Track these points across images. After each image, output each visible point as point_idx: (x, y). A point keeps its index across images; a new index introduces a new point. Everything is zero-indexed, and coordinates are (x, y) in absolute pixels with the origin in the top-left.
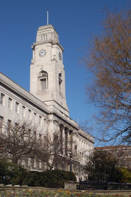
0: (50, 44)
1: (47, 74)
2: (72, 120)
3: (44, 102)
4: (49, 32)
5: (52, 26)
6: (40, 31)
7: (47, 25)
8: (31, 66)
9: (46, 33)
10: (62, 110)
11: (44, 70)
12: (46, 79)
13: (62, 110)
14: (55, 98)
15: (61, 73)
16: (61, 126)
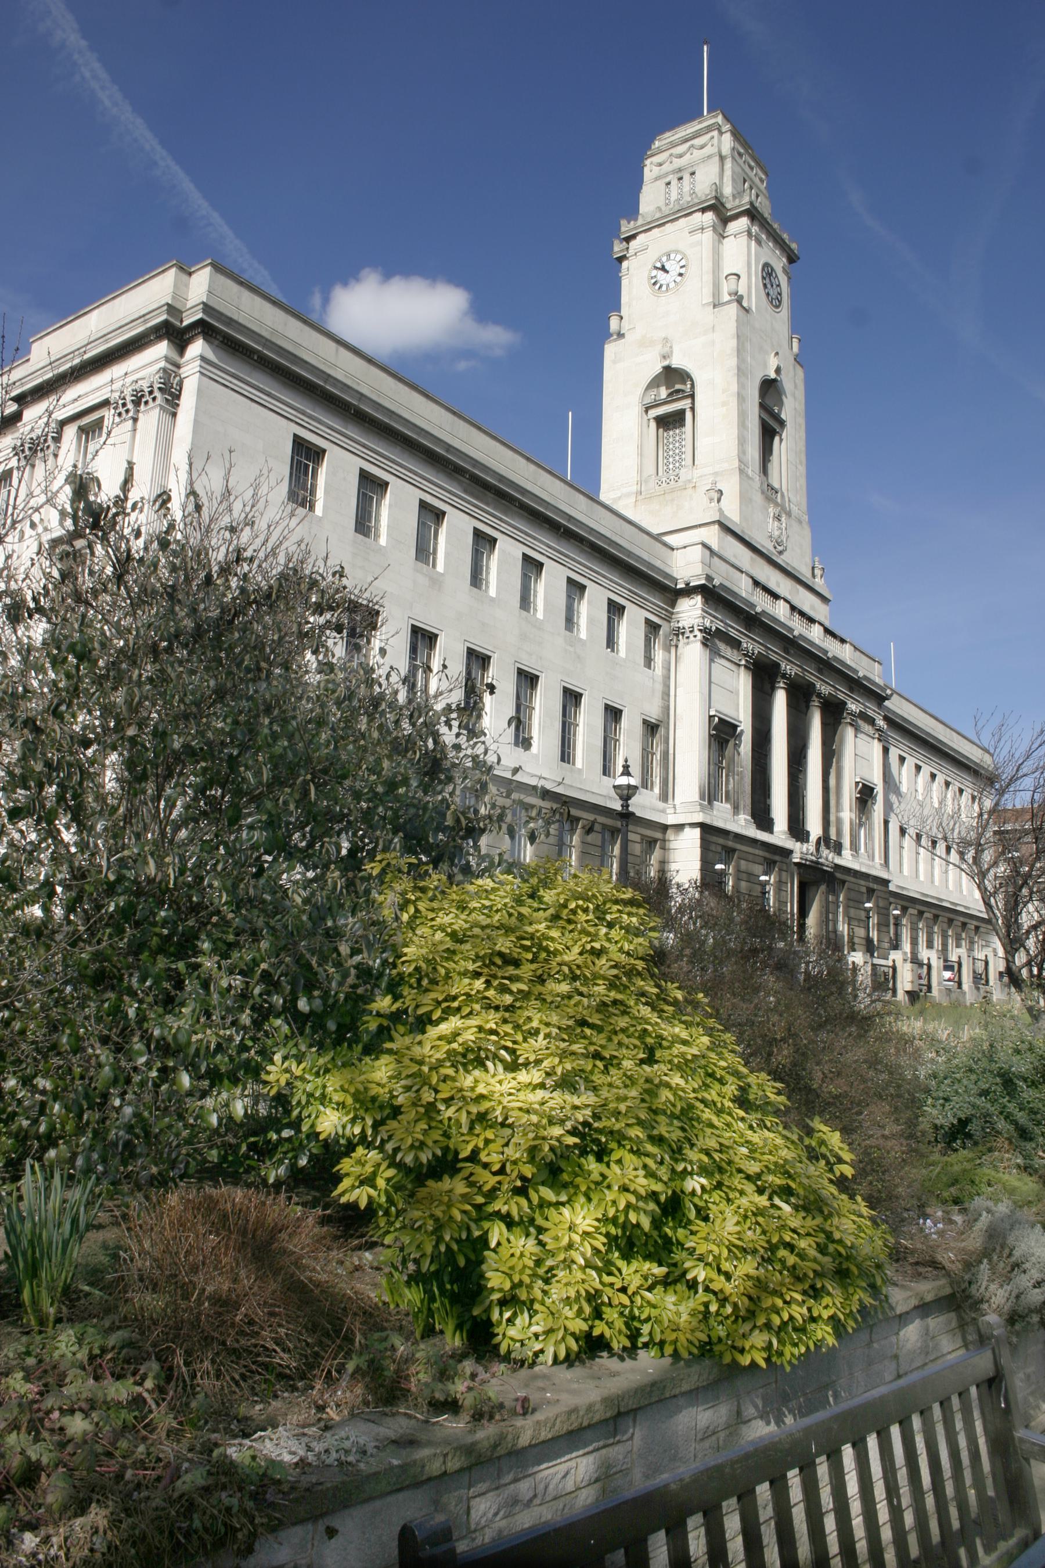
0: (710, 216)
1: (693, 386)
2: (843, 641)
3: (667, 539)
4: (708, 150)
5: (725, 117)
6: (656, 159)
7: (701, 114)
8: (611, 350)
9: (694, 160)
10: (807, 602)
11: (676, 362)
12: (681, 413)
13: (807, 602)
15: (773, 375)
16: (764, 677)
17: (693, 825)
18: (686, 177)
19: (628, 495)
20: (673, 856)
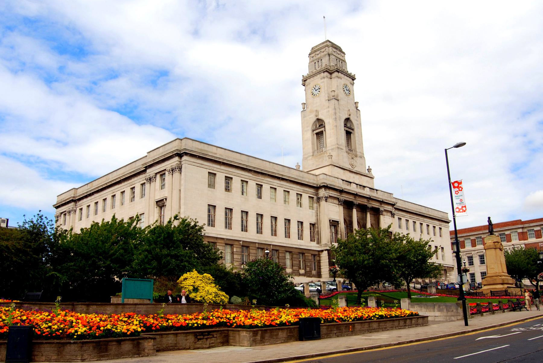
4: (325, 53)
11: (320, 117)
12: (322, 131)
14: (335, 160)
16: (348, 206)
17: (325, 250)
18: (320, 61)
19: (310, 156)
20: (322, 259)
